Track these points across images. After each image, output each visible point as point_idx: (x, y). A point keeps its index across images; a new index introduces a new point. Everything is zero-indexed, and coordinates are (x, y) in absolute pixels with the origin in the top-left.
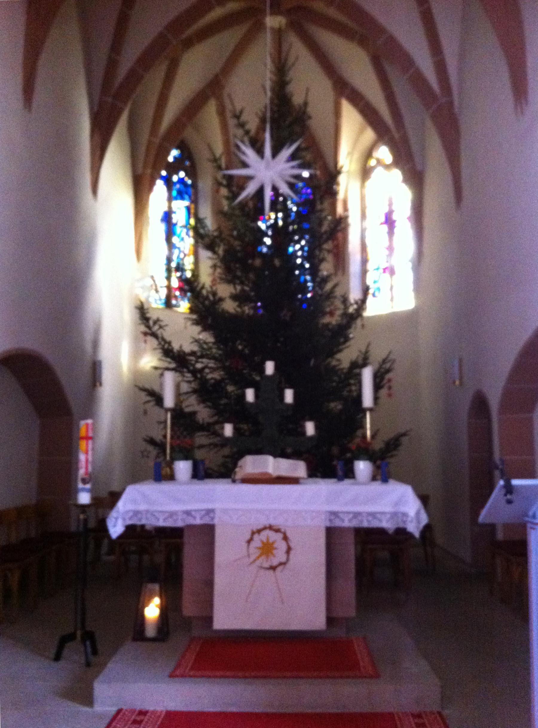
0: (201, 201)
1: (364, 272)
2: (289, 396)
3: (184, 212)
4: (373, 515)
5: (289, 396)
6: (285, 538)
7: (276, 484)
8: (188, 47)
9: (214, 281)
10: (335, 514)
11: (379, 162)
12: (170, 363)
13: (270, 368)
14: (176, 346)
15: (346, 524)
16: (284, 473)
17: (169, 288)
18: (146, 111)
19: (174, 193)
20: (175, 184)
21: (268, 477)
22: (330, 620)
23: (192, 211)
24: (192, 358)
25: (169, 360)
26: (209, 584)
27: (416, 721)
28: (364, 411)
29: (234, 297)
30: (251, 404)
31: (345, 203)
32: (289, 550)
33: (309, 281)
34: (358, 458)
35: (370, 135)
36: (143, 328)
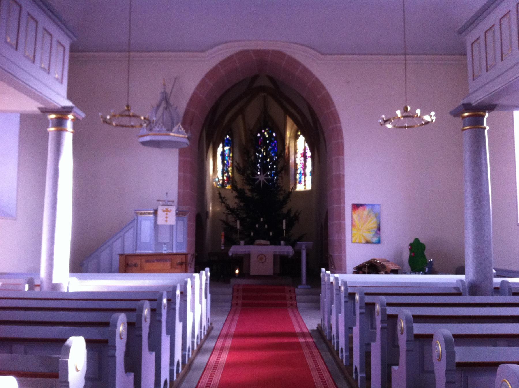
2: (266, 226)
4: (283, 252)
5: (266, 226)
6: (265, 257)
9: (243, 185)
10: (275, 251)
12: (228, 211)
13: (262, 220)
14: (231, 207)
15: (278, 254)
16: (265, 243)
17: (223, 180)
19: (225, 144)
20: (225, 140)
22: (274, 273)
23: (231, 150)
25: (228, 210)
26: (249, 266)
27: (327, 386)
28: (283, 230)
29: (249, 190)
30: (257, 228)
32: (266, 259)
33: (273, 156)
34: (282, 241)
36: (220, 200)
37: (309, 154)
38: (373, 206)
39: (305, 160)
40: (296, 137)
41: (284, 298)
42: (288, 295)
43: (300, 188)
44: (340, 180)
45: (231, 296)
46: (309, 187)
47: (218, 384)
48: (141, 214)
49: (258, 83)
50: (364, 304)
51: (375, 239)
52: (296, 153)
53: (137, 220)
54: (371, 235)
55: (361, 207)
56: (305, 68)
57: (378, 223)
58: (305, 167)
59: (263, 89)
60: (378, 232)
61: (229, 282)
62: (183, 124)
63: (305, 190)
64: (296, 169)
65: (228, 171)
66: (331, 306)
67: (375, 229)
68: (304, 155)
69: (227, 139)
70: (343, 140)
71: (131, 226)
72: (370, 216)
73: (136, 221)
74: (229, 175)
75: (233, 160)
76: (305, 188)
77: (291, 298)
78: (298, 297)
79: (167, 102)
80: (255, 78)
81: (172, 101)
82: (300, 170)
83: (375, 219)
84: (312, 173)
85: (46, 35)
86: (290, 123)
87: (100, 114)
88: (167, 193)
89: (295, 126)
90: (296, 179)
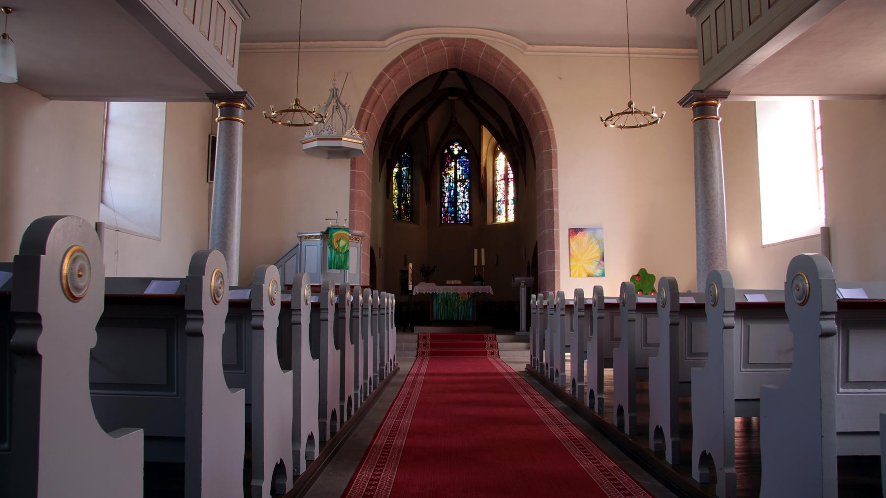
17: (399, 209)
31: (485, 168)
37: (511, 176)
38: (594, 230)
39: (507, 185)
40: (495, 155)
41: (484, 346)
42: (488, 343)
43: (501, 219)
44: (550, 198)
45: (416, 344)
46: (511, 218)
47: (418, 389)
48: (306, 238)
49: (447, 84)
50: (584, 306)
51: (599, 272)
52: (494, 175)
53: (301, 245)
54: (593, 267)
55: (580, 232)
56: (507, 60)
57: (602, 252)
58: (506, 192)
59: (452, 91)
60: (602, 262)
61: (413, 331)
62: (357, 127)
63: (507, 222)
64: (495, 195)
65: (406, 199)
66: (544, 332)
67: (598, 260)
68: (506, 179)
69: (405, 157)
70: (556, 148)
71: (293, 252)
72: (591, 244)
73: (299, 247)
74: (408, 203)
75: (412, 184)
76: (506, 220)
77: (491, 346)
78: (500, 345)
79: (338, 101)
80: (443, 74)
81: (343, 100)
82: (500, 196)
83: (598, 247)
84: (516, 200)
85: (221, 10)
86: (486, 134)
87: (264, 112)
88: (337, 212)
89: (494, 140)
90: (494, 209)
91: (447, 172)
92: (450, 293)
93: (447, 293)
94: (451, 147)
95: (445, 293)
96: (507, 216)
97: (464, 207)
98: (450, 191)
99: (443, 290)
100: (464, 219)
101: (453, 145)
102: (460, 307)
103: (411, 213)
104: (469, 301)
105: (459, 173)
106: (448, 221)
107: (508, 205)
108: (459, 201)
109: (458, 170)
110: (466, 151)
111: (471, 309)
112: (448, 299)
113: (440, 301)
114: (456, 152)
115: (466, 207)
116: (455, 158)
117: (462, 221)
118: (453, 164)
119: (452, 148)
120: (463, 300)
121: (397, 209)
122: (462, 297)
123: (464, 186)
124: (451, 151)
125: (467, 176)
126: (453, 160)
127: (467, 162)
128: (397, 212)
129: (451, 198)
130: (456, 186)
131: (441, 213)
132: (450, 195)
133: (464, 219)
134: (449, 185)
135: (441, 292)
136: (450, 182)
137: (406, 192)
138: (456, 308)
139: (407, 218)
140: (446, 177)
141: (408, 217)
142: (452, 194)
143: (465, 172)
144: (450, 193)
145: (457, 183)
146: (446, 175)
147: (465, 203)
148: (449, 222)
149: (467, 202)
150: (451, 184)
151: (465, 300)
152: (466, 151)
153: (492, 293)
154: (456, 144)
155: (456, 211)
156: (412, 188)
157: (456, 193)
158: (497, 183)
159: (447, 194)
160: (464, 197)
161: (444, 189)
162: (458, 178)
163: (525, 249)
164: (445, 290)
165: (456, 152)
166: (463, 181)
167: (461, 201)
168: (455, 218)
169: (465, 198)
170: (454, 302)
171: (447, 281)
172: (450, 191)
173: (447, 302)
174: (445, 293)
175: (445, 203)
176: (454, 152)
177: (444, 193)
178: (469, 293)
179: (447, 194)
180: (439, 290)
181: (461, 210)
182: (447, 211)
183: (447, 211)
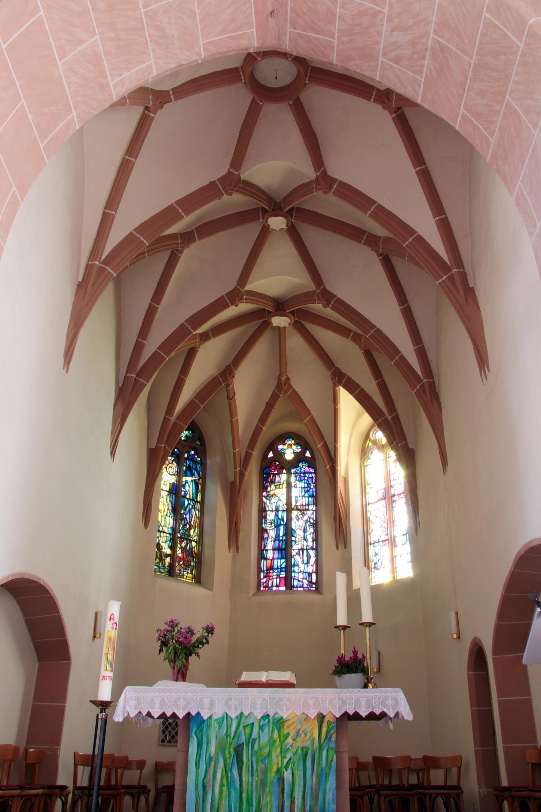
0: (210, 485)
1: (366, 544)
3: (192, 485)
7: (256, 186)
8: (205, 341)
11: (375, 442)
17: (173, 556)
18: (184, 631)
21: (262, 683)
24: (181, 517)
31: (346, 480)
35: (367, 419)
58: (391, 522)
65: (187, 538)
75: (202, 511)
91: (272, 493)
92: (250, 714)
93: (242, 714)
94: (280, 447)
95: (233, 714)
96: (394, 570)
97: (305, 558)
98: (277, 526)
99: (227, 704)
100: (305, 581)
101: (285, 444)
102: (287, 775)
103: (199, 567)
104: (321, 748)
105: (296, 492)
106: (272, 586)
107: (395, 546)
108: (296, 547)
109: (293, 489)
110: (308, 454)
111: (331, 783)
112: (243, 739)
113: (213, 749)
114: (289, 456)
115: (309, 557)
116: (289, 466)
117: (302, 586)
118: (284, 477)
119: (282, 449)
120: (299, 744)
121: (167, 555)
122: (298, 733)
123: (306, 518)
124: (279, 455)
125: (311, 499)
126: (284, 471)
127: (311, 473)
128: (168, 560)
129: (279, 541)
130: (289, 519)
131: (260, 570)
132: (277, 536)
133: (305, 581)
134: (277, 515)
135: (218, 713)
136: (277, 510)
137: (190, 525)
138: (272, 775)
139: (188, 576)
140: (270, 501)
141: (190, 575)
142: (281, 534)
143: (306, 492)
144: (278, 531)
145: (291, 512)
146: (269, 497)
147: (307, 549)
148: (274, 588)
149: (312, 549)
150: (280, 514)
151: (308, 743)
152: (308, 454)
153: (407, 715)
154: (290, 442)
155: (288, 568)
156: (201, 518)
157: (289, 532)
158: (369, 508)
159: (272, 533)
160: (305, 539)
161: (265, 523)
162: (294, 503)
163: (457, 614)
164: (232, 703)
165: (289, 456)
166: (303, 510)
167: (299, 547)
168: (288, 581)
169: (307, 541)
170: (266, 751)
171: (244, 673)
172: (277, 526)
173: (238, 751)
174: (233, 714)
175: (267, 550)
176: (286, 455)
177: (266, 531)
178: (321, 717)
179: (272, 533)
180: (212, 705)
181: (300, 564)
182: (271, 568)
183: (271, 568)
